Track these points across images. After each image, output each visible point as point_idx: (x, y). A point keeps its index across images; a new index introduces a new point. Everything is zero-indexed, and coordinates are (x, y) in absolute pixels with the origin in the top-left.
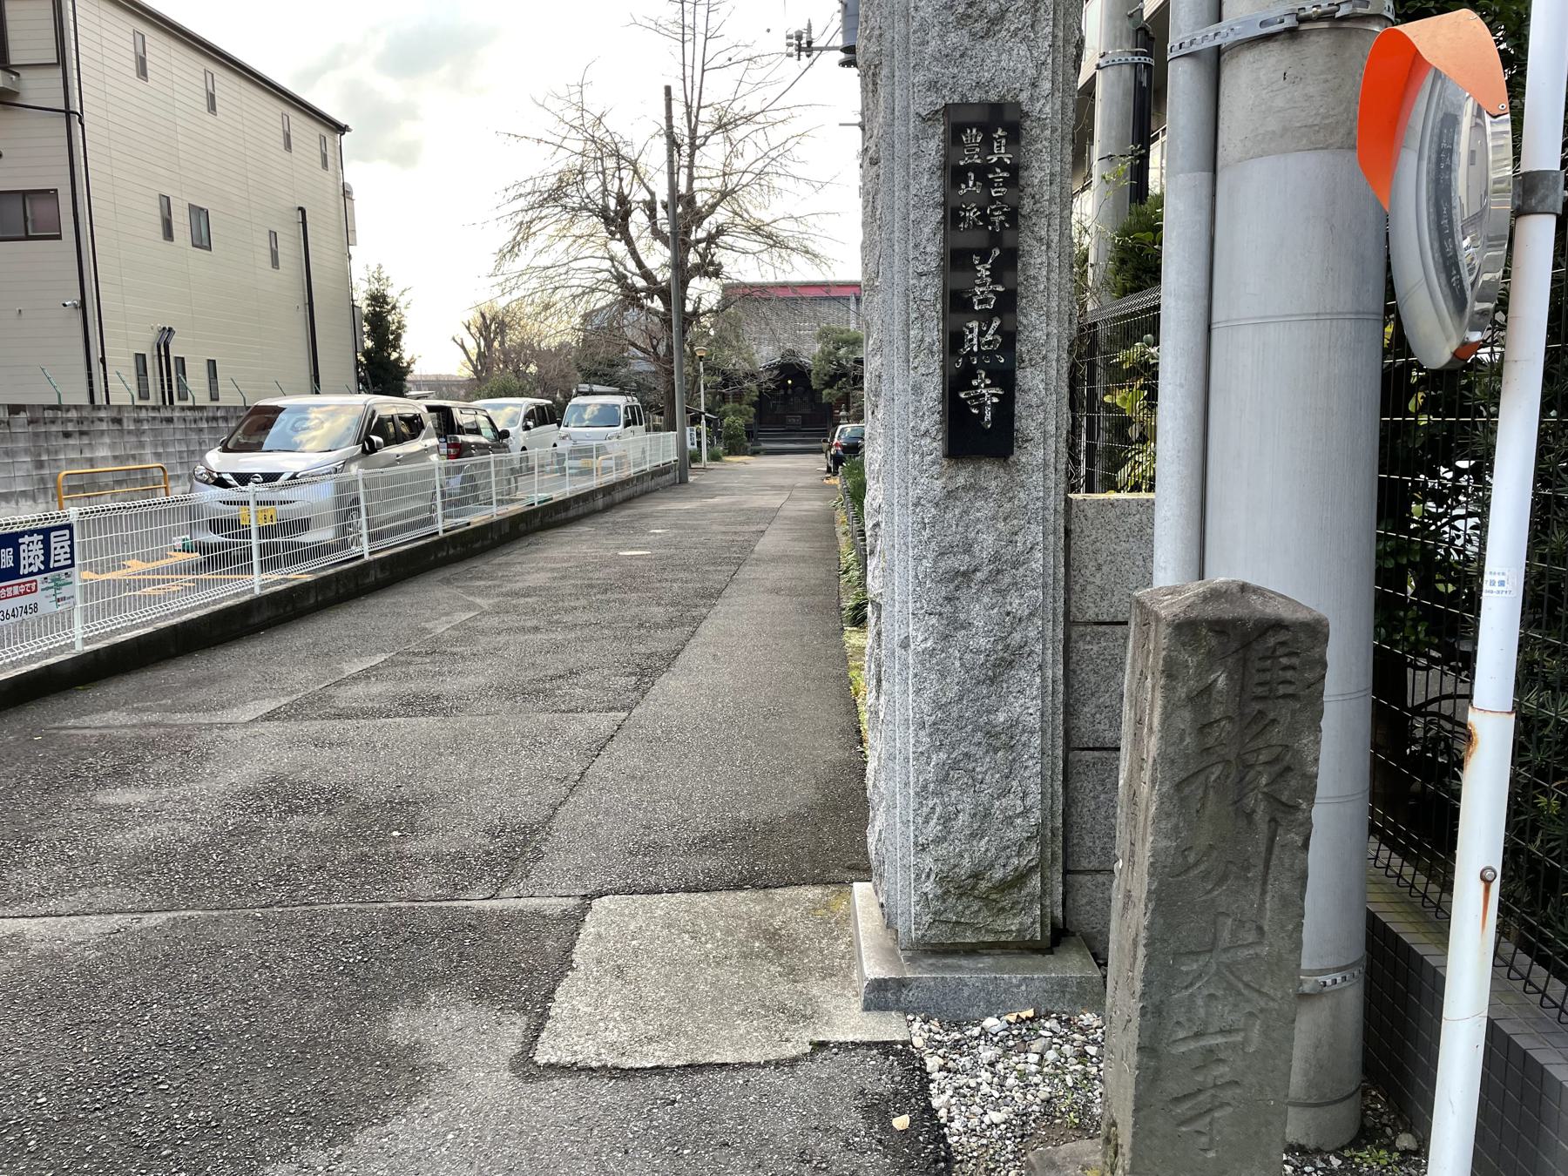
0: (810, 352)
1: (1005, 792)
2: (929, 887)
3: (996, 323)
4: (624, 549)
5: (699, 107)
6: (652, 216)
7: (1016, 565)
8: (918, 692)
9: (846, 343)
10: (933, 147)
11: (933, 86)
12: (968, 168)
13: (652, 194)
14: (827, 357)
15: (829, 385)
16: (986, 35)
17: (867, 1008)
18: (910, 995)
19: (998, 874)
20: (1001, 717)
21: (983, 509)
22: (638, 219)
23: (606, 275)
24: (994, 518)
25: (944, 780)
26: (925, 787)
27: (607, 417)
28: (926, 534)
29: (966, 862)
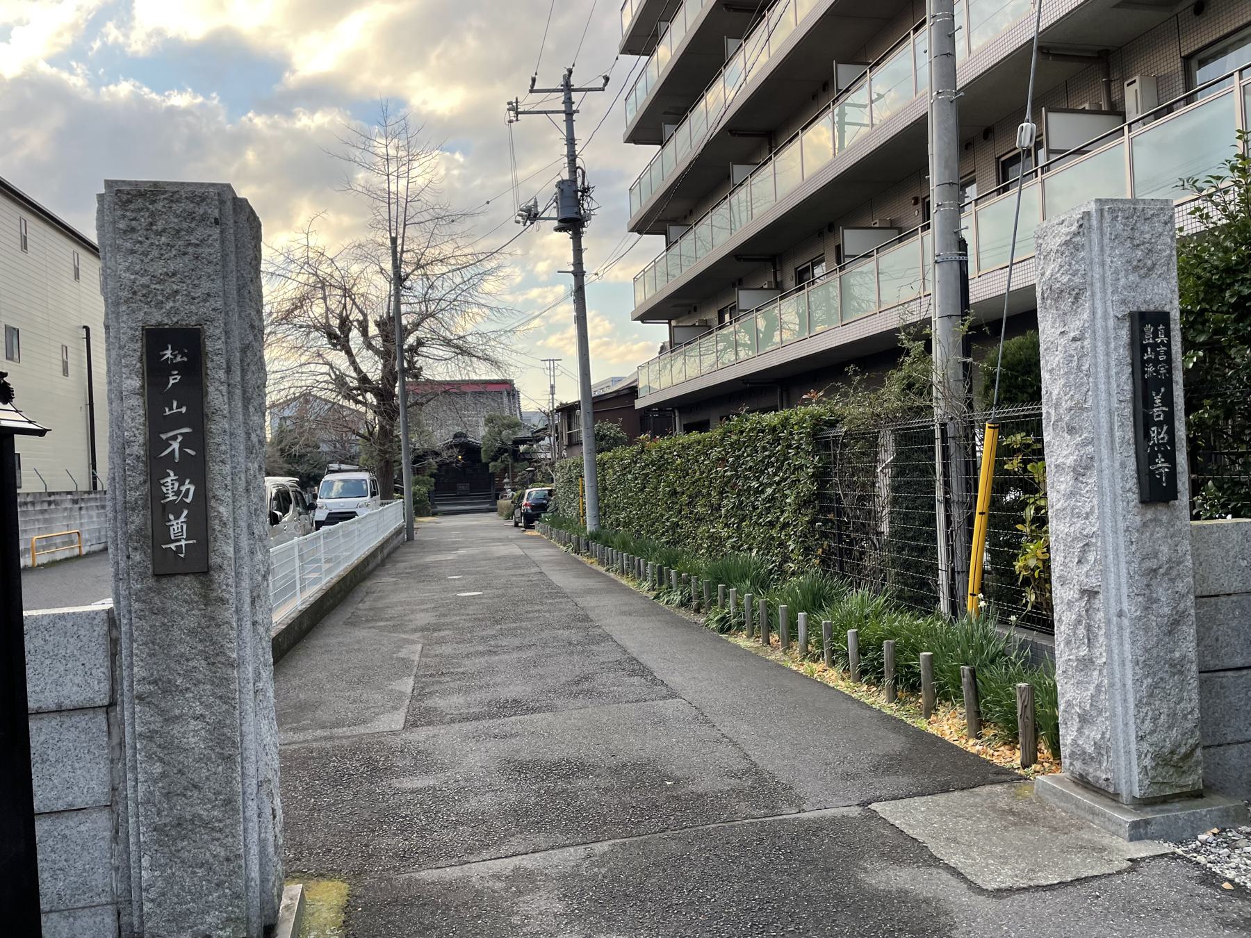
0: (480, 433)
1: (1181, 700)
2: (1147, 762)
3: (1165, 428)
4: (464, 591)
5: (403, 251)
6: (364, 332)
7: (1179, 563)
8: (1133, 643)
9: (509, 426)
10: (1125, 334)
11: (1124, 302)
12: (1149, 345)
13: (365, 316)
14: (493, 436)
15: (495, 459)
16: (1147, 275)
17: (1131, 840)
18: (1151, 829)
19: (1183, 750)
20: (1177, 654)
21: (1160, 532)
22: (355, 334)
23: (327, 378)
24: (1166, 537)
25: (1151, 695)
26: (1140, 701)
27: (352, 489)
28: (1134, 548)
29: (1168, 744)
